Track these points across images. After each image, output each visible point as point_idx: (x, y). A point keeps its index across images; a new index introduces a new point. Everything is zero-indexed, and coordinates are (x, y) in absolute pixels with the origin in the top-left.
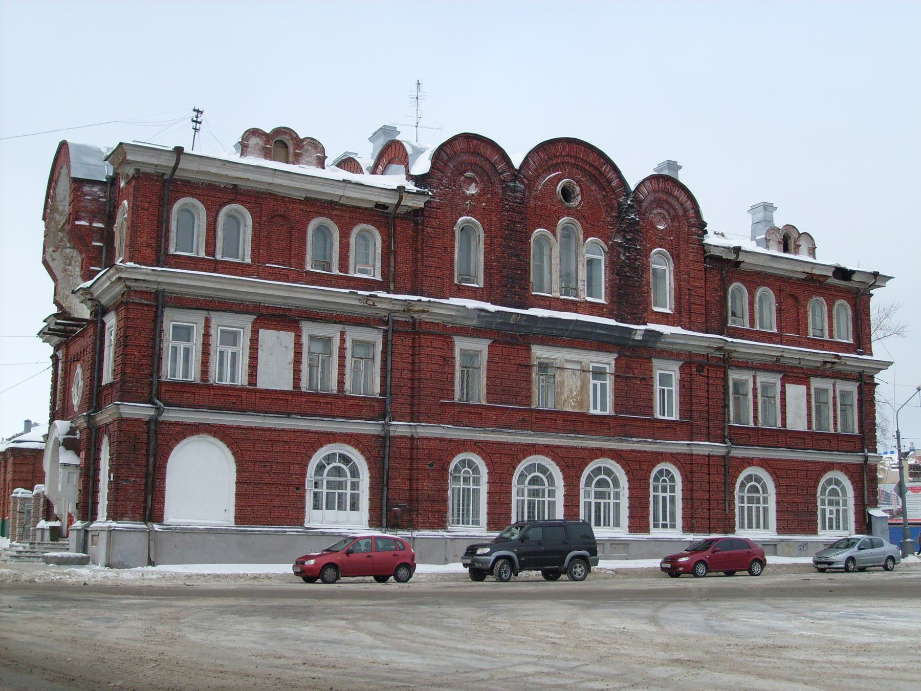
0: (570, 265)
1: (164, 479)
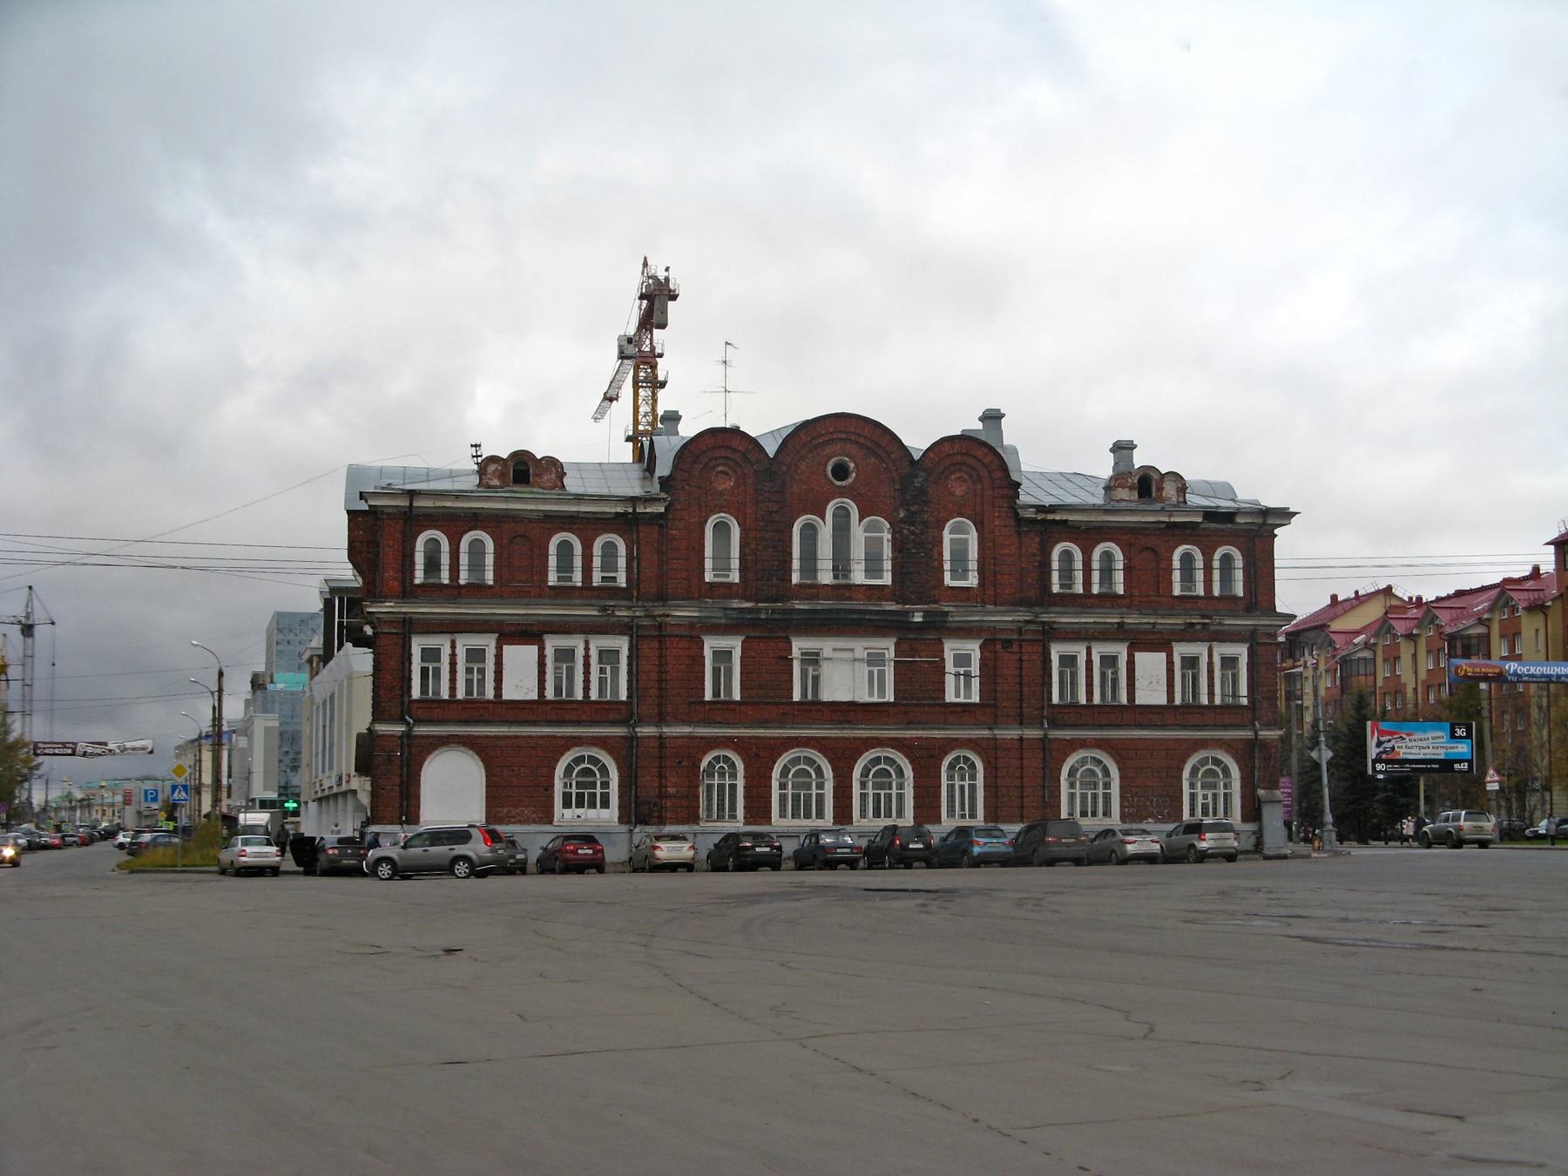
0: (847, 546)
1: (419, 786)
